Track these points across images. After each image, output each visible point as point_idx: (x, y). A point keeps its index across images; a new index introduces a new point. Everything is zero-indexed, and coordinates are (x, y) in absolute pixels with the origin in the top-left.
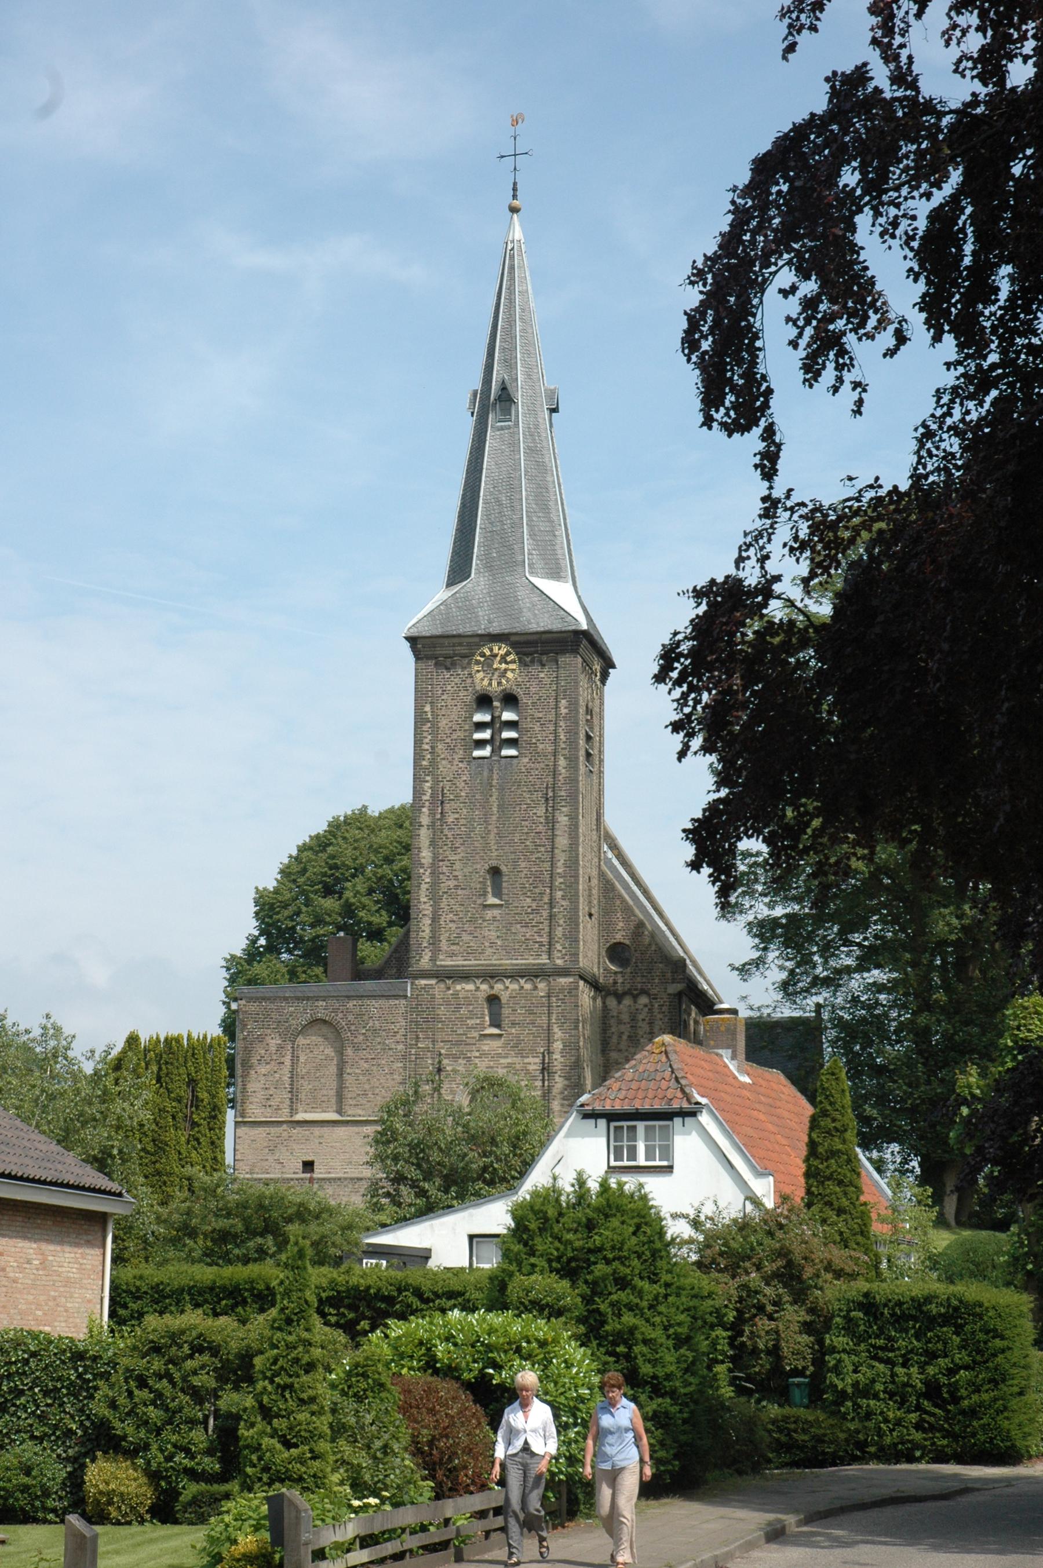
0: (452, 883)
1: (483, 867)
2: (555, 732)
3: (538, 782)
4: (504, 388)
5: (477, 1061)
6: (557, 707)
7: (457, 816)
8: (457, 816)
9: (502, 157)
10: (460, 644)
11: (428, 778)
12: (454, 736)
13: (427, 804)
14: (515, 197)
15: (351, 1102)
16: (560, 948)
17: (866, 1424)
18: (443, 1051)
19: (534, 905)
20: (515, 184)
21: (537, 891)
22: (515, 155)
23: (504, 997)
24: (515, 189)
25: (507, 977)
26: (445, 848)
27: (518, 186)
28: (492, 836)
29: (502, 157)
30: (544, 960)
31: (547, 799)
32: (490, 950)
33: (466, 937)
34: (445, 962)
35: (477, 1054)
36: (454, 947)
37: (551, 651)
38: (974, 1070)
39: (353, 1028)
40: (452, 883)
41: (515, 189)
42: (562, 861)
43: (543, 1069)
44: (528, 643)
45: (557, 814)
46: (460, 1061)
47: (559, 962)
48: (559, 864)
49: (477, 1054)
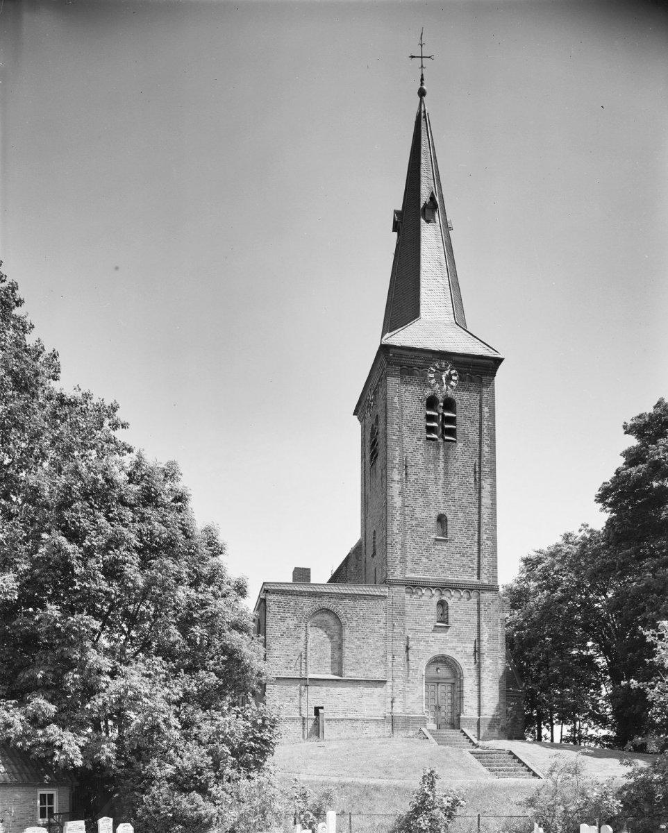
0: (414, 523)
1: (434, 515)
2: (480, 427)
3: (470, 460)
4: (432, 198)
5: (432, 644)
6: (481, 411)
7: (416, 477)
8: (416, 477)
9: (413, 57)
10: (419, 358)
11: (397, 449)
12: (414, 422)
13: (397, 466)
14: (422, 84)
15: (348, 667)
16: (486, 572)
17: (15, 623)
18: (410, 636)
19: (468, 542)
20: (422, 75)
21: (470, 533)
22: (422, 57)
23: (450, 603)
24: (422, 79)
25: (453, 589)
26: (409, 498)
27: (425, 78)
28: (440, 494)
29: (413, 57)
30: (475, 579)
31: (475, 472)
32: (440, 570)
33: (424, 560)
34: (410, 575)
35: (433, 639)
36: (416, 566)
37: (478, 373)
38: (597, 660)
39: (349, 616)
40: (414, 523)
41: (422, 79)
42: (486, 515)
43: (475, 651)
44: (465, 364)
45: (483, 482)
46: (422, 643)
47: (486, 582)
48: (484, 516)
49: (433, 639)
